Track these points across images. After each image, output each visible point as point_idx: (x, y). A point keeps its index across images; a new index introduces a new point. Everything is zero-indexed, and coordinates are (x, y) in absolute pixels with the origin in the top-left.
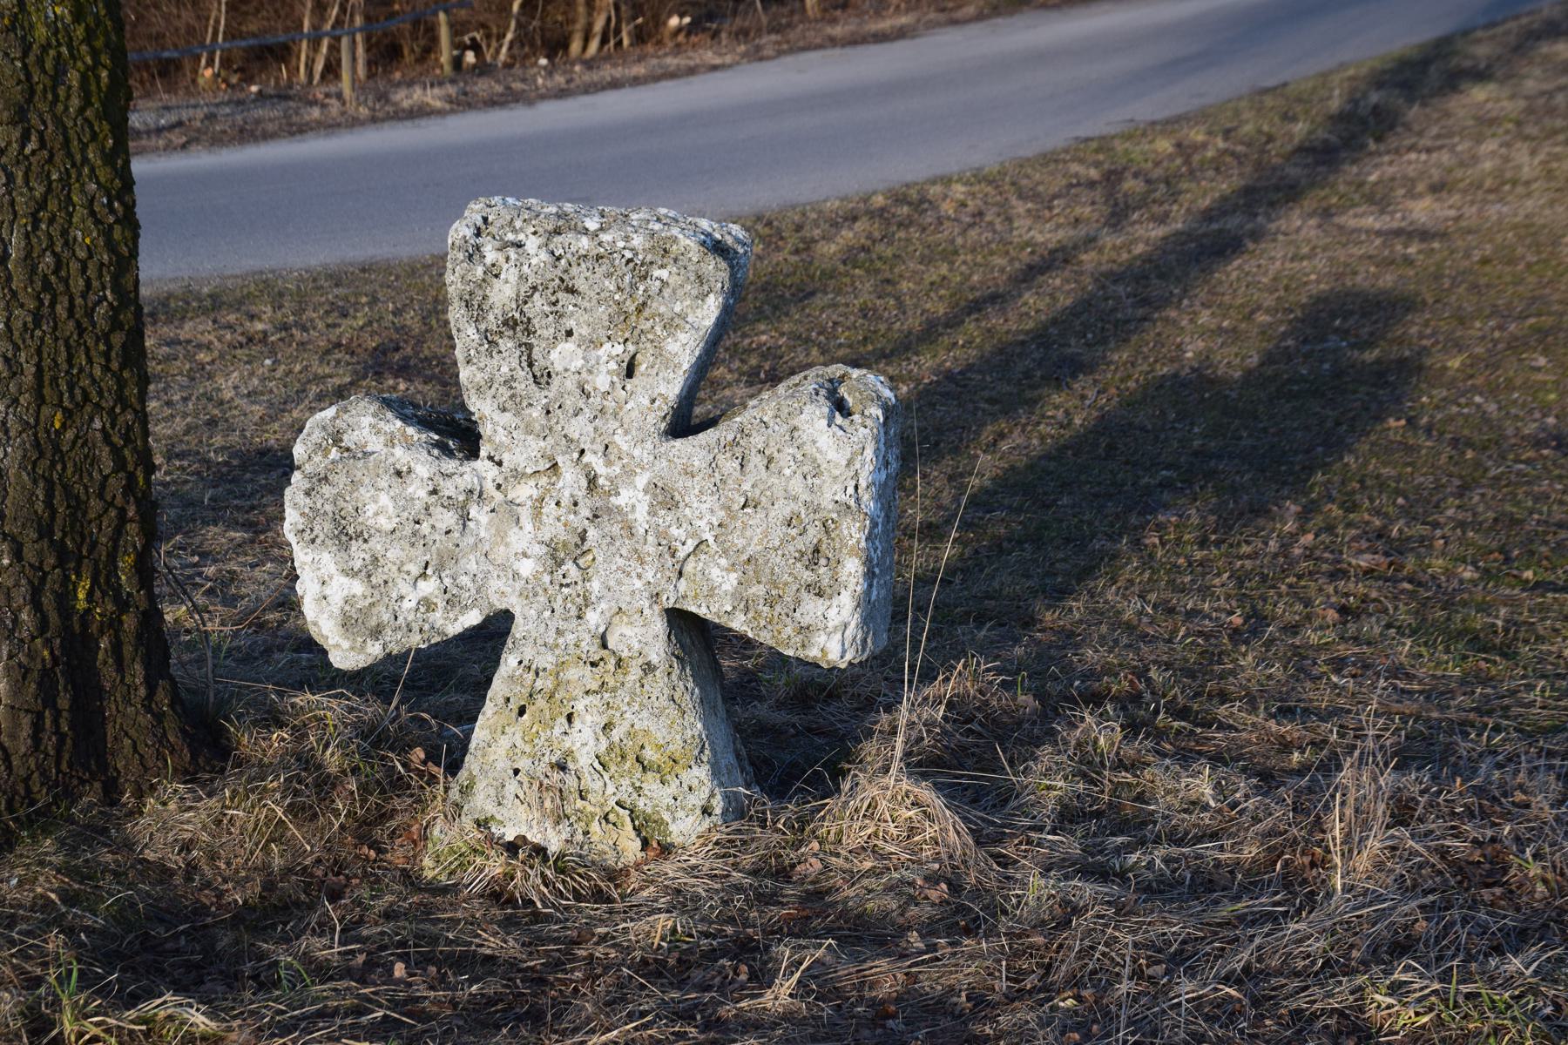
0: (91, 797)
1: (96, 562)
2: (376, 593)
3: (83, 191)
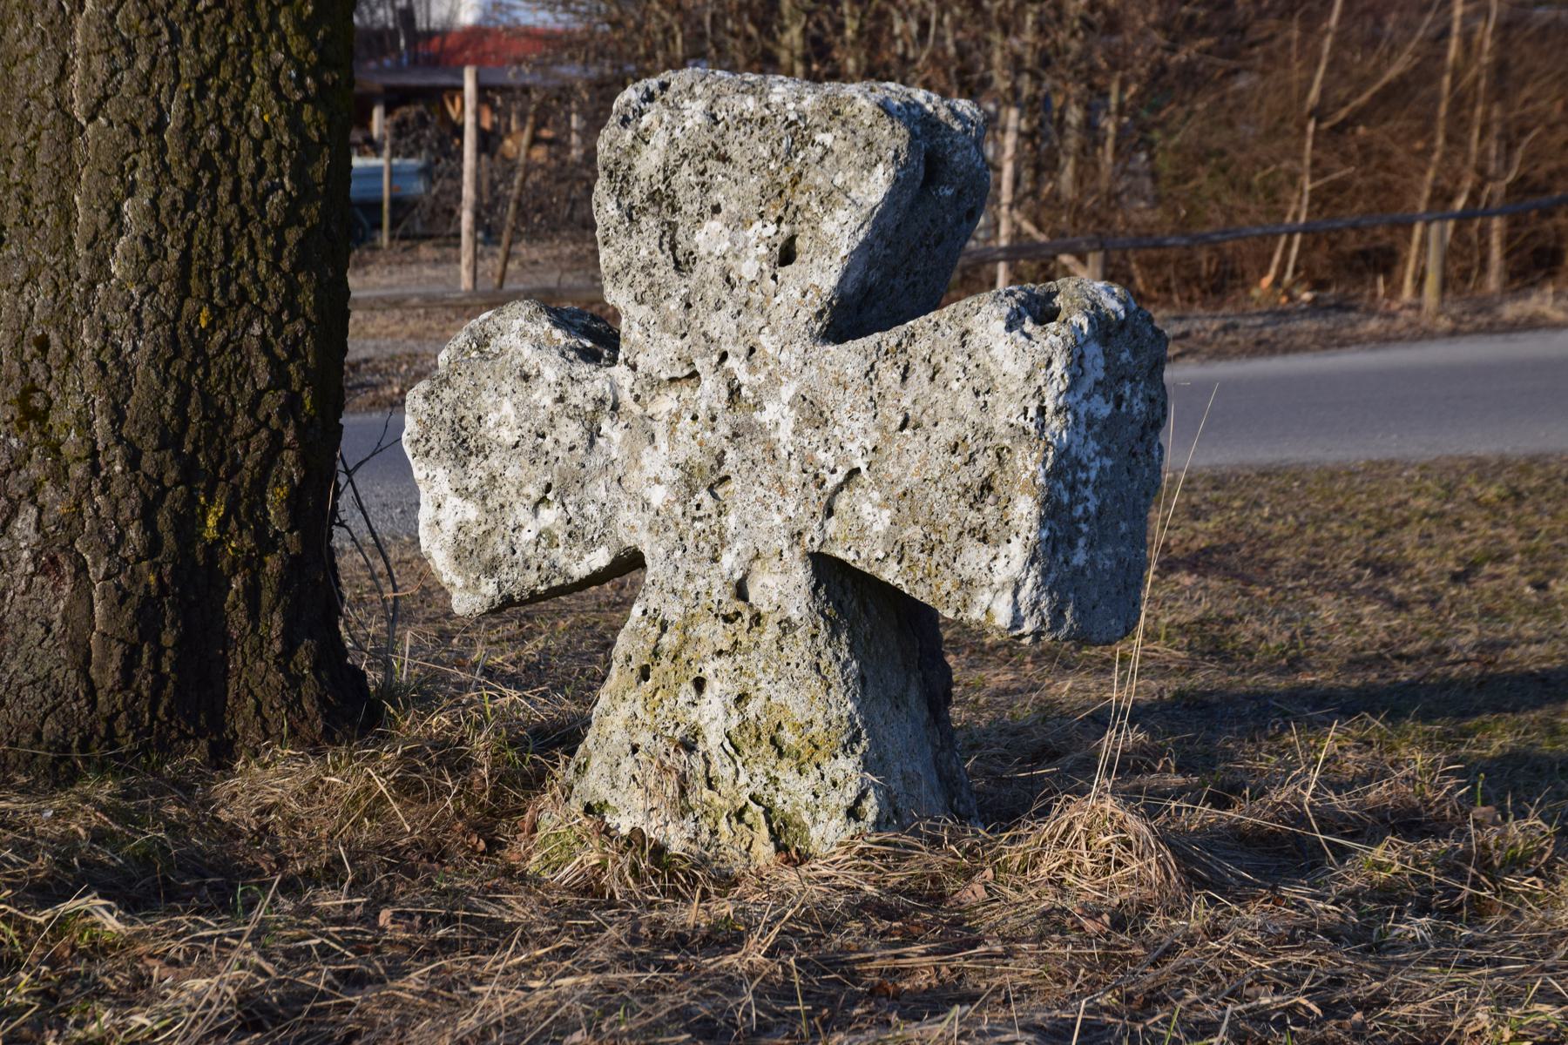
0: (196, 755)
1: (235, 489)
2: (490, 518)
3: (266, 57)
